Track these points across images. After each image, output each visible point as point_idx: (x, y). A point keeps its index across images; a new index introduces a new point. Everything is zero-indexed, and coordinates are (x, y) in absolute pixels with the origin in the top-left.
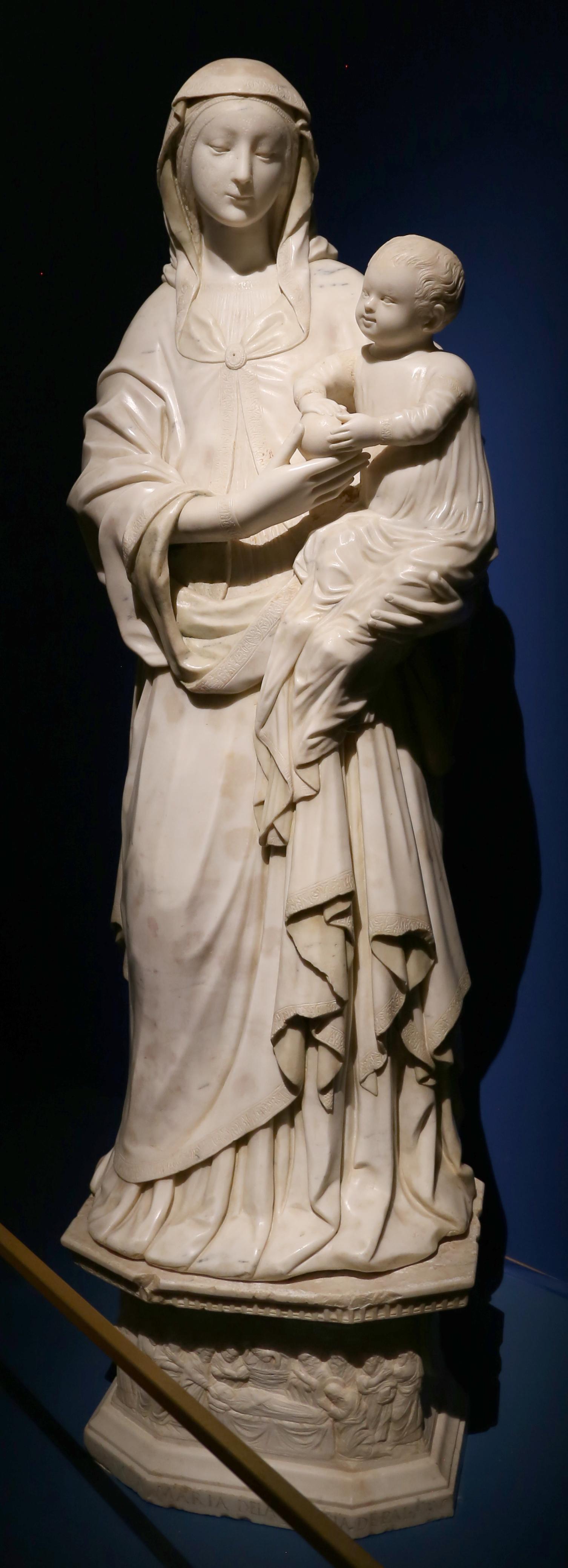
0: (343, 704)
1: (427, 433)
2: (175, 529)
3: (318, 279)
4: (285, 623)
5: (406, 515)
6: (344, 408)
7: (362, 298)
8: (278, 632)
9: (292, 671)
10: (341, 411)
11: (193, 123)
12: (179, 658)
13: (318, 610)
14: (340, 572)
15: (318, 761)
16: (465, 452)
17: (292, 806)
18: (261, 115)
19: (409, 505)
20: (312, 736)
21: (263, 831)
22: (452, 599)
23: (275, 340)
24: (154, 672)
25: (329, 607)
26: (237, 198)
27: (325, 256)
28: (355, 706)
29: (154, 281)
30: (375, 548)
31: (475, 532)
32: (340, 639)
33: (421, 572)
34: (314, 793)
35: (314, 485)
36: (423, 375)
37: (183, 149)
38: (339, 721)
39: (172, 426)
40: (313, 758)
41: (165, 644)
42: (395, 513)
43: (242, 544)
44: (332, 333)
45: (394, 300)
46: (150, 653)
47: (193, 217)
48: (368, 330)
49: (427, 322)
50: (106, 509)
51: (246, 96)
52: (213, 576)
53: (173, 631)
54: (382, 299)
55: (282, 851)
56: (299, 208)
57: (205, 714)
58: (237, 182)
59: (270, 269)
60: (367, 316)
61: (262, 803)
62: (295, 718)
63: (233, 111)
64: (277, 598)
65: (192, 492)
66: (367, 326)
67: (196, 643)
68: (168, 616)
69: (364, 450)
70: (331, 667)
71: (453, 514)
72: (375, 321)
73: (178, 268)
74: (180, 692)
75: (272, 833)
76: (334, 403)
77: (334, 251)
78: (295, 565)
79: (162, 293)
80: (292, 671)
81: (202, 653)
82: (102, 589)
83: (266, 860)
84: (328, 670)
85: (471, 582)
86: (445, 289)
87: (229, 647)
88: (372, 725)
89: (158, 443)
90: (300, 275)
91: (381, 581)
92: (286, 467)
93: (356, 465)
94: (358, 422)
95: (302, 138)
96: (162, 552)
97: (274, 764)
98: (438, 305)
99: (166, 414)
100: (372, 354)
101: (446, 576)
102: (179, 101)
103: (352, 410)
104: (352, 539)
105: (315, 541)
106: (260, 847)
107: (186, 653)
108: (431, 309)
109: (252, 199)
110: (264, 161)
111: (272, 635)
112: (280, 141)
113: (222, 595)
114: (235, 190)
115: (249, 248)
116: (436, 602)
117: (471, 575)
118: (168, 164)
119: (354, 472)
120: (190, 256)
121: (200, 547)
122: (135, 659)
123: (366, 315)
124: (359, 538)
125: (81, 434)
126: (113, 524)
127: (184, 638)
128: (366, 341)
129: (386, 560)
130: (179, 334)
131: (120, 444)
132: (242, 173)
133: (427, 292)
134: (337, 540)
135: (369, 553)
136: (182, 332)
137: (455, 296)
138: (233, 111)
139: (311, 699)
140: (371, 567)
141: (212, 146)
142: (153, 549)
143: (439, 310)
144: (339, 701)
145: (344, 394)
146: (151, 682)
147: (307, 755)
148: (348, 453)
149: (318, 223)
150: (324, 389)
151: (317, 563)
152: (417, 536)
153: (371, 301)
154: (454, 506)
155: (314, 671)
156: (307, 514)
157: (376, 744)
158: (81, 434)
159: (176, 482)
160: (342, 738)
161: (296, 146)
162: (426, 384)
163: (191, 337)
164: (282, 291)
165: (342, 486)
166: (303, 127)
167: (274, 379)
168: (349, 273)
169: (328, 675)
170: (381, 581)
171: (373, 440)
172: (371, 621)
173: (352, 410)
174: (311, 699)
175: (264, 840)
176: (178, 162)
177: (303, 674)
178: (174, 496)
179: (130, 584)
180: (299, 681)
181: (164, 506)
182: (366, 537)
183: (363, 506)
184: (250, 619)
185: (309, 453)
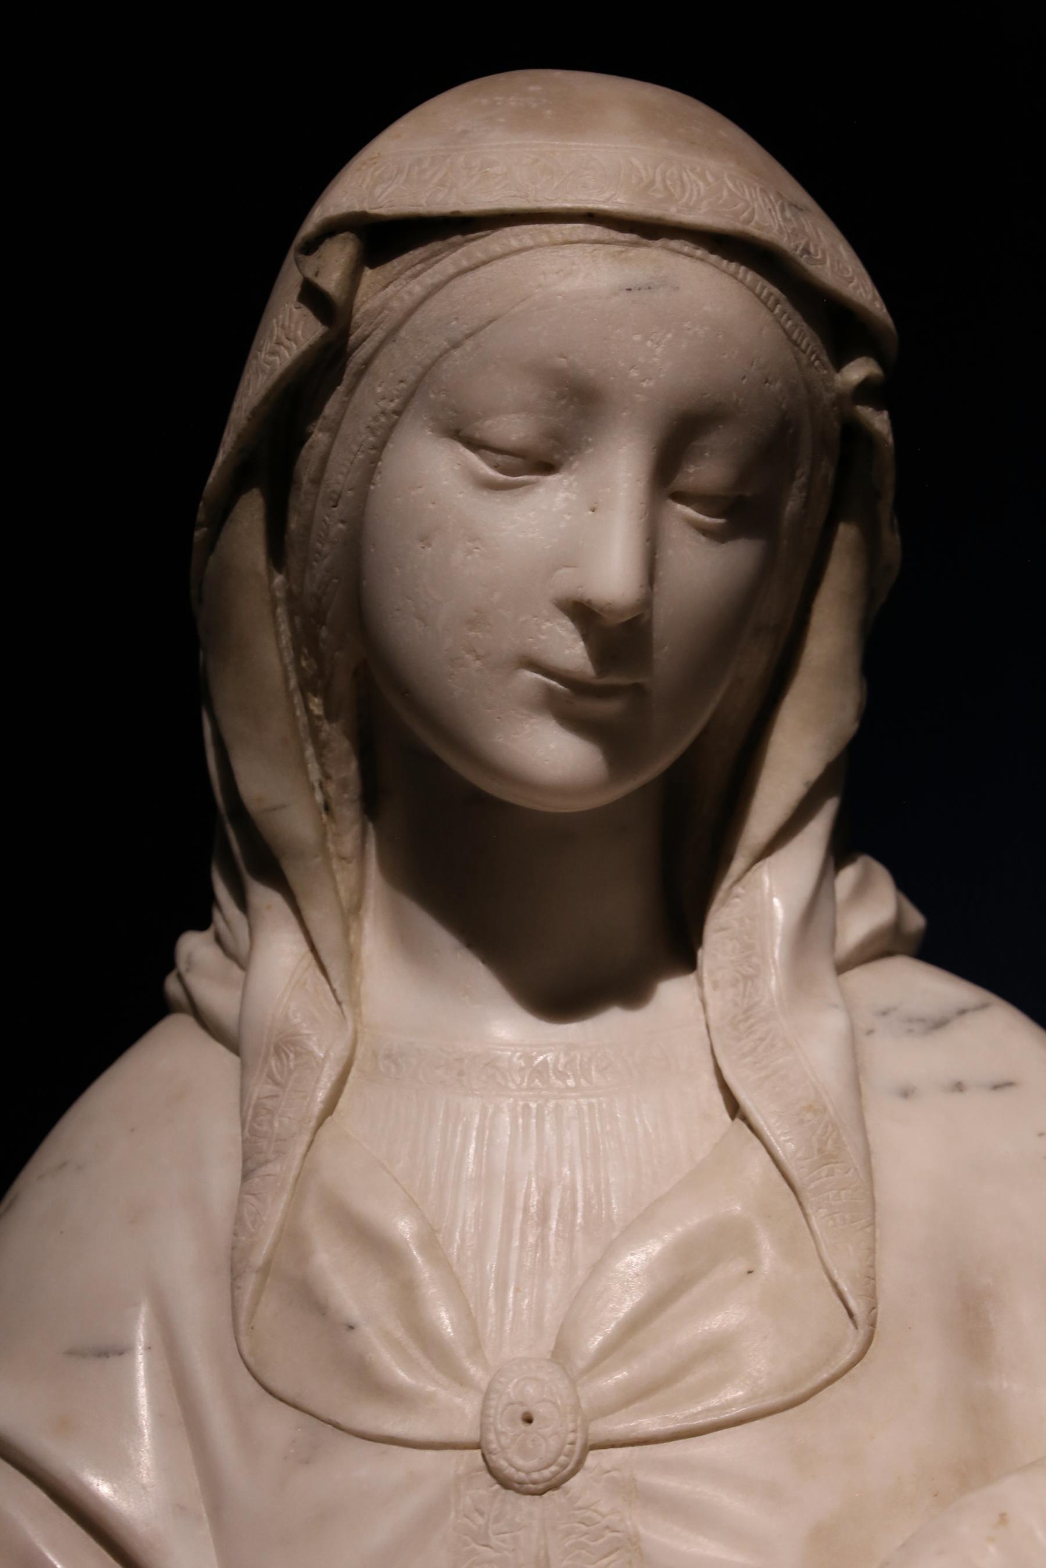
11: (392, 335)
18: (693, 323)
26: (576, 685)
29: (130, 1001)
37: (331, 447)
47: (341, 745)
56: (797, 752)
58: (582, 613)
59: (673, 994)
73: (259, 964)
77: (916, 920)
79: (166, 1061)
90: (817, 1042)
95: (854, 433)
102: (332, 229)
109: (638, 691)
110: (704, 531)
112: (773, 450)
114: (570, 650)
118: (250, 514)
120: (314, 915)
130: (250, 1283)
132: (613, 575)
136: (266, 1270)
141: (475, 445)
149: (870, 811)
161: (828, 470)
163: (312, 1302)
164: (734, 1108)
166: (865, 392)
176: (300, 503)
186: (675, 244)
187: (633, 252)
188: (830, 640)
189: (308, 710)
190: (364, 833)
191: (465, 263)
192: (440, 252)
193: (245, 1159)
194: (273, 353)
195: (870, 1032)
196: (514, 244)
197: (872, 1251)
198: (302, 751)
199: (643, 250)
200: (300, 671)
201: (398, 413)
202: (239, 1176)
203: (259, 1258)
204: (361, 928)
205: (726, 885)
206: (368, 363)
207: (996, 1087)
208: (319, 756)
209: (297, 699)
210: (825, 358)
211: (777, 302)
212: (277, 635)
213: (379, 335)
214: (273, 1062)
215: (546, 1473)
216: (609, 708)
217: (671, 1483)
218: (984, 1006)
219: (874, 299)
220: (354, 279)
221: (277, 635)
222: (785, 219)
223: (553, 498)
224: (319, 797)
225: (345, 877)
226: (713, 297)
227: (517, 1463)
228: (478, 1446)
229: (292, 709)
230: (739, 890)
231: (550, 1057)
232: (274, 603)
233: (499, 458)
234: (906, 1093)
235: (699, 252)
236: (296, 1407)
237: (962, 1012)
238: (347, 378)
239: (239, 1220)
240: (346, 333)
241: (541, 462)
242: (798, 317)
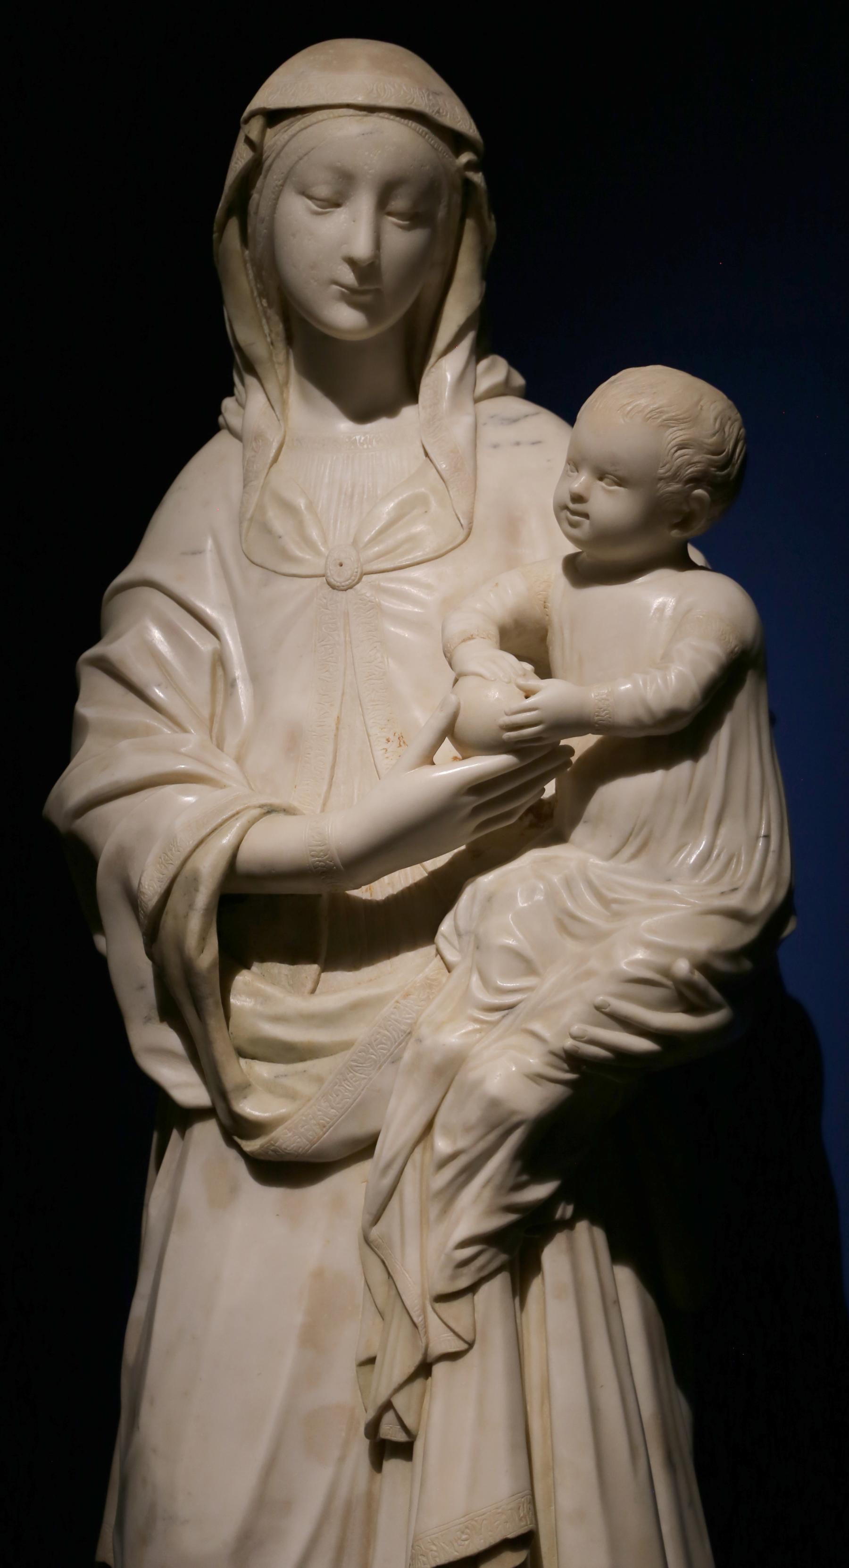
0: (518, 1187)
1: (673, 715)
2: (232, 870)
3: (491, 433)
4: (419, 1041)
5: (635, 856)
6: (529, 667)
7: (565, 475)
8: (407, 1056)
9: (429, 1127)
10: (524, 675)
11: (278, 155)
12: (232, 1096)
13: (476, 1020)
14: (517, 955)
15: (472, 1289)
16: (741, 747)
17: (424, 1369)
18: (389, 145)
19: (640, 840)
20: (463, 1244)
21: (371, 1414)
22: (713, 1007)
23: (413, 540)
24: (188, 1117)
25: (496, 1016)
26: (352, 291)
27: (503, 390)
28: (539, 1192)
29: (207, 426)
30: (579, 913)
31: (755, 889)
32: (513, 1073)
33: (661, 960)
34: (465, 1346)
35: (474, 801)
36: (668, 612)
37: (260, 199)
38: (511, 1217)
39: (231, 685)
40: (463, 1282)
41: (204, 1060)
42: (616, 853)
43: (348, 896)
44: (512, 528)
45: (621, 482)
46: (184, 1085)
47: (276, 318)
48: (575, 532)
50: (113, 830)
51: (371, 110)
52: (295, 952)
53: (222, 1048)
54: (601, 479)
55: (404, 1450)
56: (456, 312)
57: (273, 1196)
58: (351, 262)
59: (408, 412)
60: (572, 508)
61: (371, 1361)
62: (434, 1210)
63: (348, 130)
64: (407, 995)
65: (261, 806)
66: (573, 525)
67: (262, 1070)
68: (215, 1022)
69: (563, 742)
70: (497, 1122)
71: (718, 855)
72: (586, 516)
73: (250, 407)
74: (232, 1154)
75: (389, 1417)
76: (512, 659)
77: (519, 380)
78: (439, 939)
80: (429, 1127)
81: (273, 1088)
82: (100, 963)
83: (377, 1464)
84: (493, 1128)
85: (749, 979)
86: (711, 463)
87: (320, 1080)
88: (568, 1224)
89: (206, 712)
90: (459, 428)
91: (589, 974)
92: (427, 770)
93: (549, 767)
94: (553, 694)
95: (468, 184)
96: (207, 911)
97: (394, 1292)
98: (699, 492)
99: (220, 661)
100: (582, 572)
101: (703, 967)
102: (253, 114)
103: (544, 670)
104: (539, 897)
105: (473, 897)
106: (366, 1442)
107: (245, 1088)
108: (686, 497)
109: (378, 292)
111: (395, 1060)
113: (310, 985)
114: (349, 277)
115: (371, 377)
116: (686, 1011)
117: (747, 965)
118: (233, 226)
119: (545, 778)
121: (273, 901)
122: (156, 1093)
123: (572, 506)
124: (552, 895)
125: (72, 692)
126: (123, 857)
127: (243, 1061)
128: (571, 549)
129: (597, 936)
130: (245, 525)
131: (140, 715)
133: (679, 468)
134: (514, 894)
135: (567, 921)
136: (251, 520)
137: (729, 475)
138: (348, 130)
139: (461, 1179)
140: (571, 946)
141: (311, 198)
142: (191, 906)
143: (699, 499)
144: (510, 1182)
145: (529, 642)
146: (183, 1134)
147: (453, 1278)
148: (536, 749)
149: (491, 334)
150: (494, 632)
151: (477, 937)
152: (654, 895)
153: (581, 481)
154: (719, 842)
155: (468, 1129)
156: (463, 847)
157: (574, 1258)
158: (71, 691)
159: (236, 790)
160: (515, 1249)
161: (457, 199)
162: (672, 628)
163: (266, 529)
164: (427, 454)
165: (526, 801)
166: (469, 166)
167: (409, 608)
168: (543, 423)
169: (492, 1137)
170: (589, 974)
171: (579, 725)
172: (569, 1043)
173: (544, 670)
174: (461, 1179)
175: (373, 1428)
176: (252, 221)
177: (448, 1132)
178: (229, 814)
179: (150, 963)
180: (442, 1145)
181: (214, 830)
182: (565, 895)
183: (559, 837)
184: (358, 1032)
185: (468, 747)
186: (381, 114)
187: (365, 119)
188: (467, 267)
189: (262, 305)
190: (288, 353)
191: (303, 126)
192: (292, 122)
193: (245, 480)
194: (236, 163)
195: (485, 424)
196: (320, 118)
197: (473, 503)
198: (260, 322)
199: (369, 118)
200: (257, 289)
201: (282, 185)
202: (242, 487)
203: (248, 516)
204: (288, 392)
205: (428, 368)
206: (270, 166)
207: (533, 444)
208: (268, 323)
209: (258, 300)
210: (450, 153)
211: (426, 134)
212: (247, 275)
213: (273, 155)
214: (254, 444)
215: (347, 583)
216: (367, 298)
217: (393, 585)
218: (537, 414)
219: (470, 128)
220: (263, 133)
221: (247, 275)
222: (429, 100)
223: (340, 217)
224: (269, 339)
225: (281, 372)
226: (399, 135)
227: (337, 580)
228: (324, 576)
229: (256, 305)
230: (433, 370)
231: (358, 437)
232: (245, 262)
233: (319, 203)
234: (495, 446)
235: (392, 117)
236: (262, 567)
237: (526, 416)
238: (263, 172)
239: (242, 503)
240: (261, 155)
241: (334, 203)
242: (437, 139)
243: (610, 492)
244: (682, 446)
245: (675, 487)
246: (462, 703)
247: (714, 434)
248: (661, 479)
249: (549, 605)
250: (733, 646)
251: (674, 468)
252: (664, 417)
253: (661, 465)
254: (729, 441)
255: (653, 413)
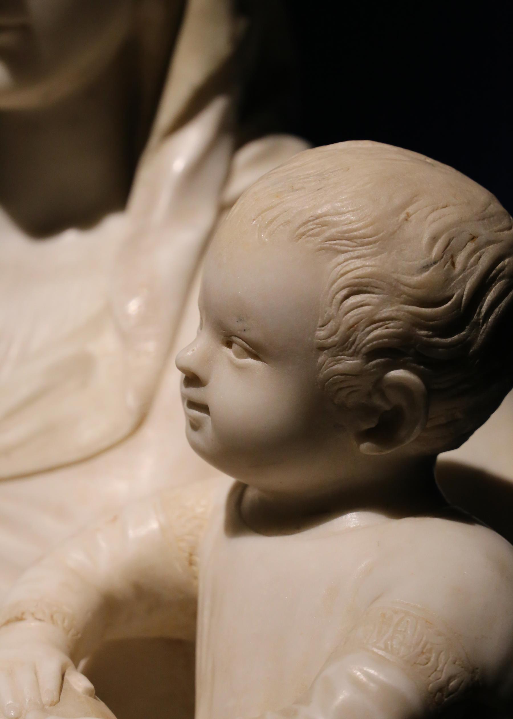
45: (255, 351)
48: (196, 436)
49: (372, 425)
54: (229, 344)
86: (419, 322)
98: (397, 374)
133: (353, 328)
137: (465, 344)
143: (400, 386)
243: (240, 368)
244: (356, 289)
245: (349, 363)
246: (185, 364)
247: (426, 267)
248: (322, 349)
249: (197, 559)
250: (443, 677)
251: (342, 329)
252: (327, 234)
253: (320, 323)
254: (464, 281)
255: (310, 226)
